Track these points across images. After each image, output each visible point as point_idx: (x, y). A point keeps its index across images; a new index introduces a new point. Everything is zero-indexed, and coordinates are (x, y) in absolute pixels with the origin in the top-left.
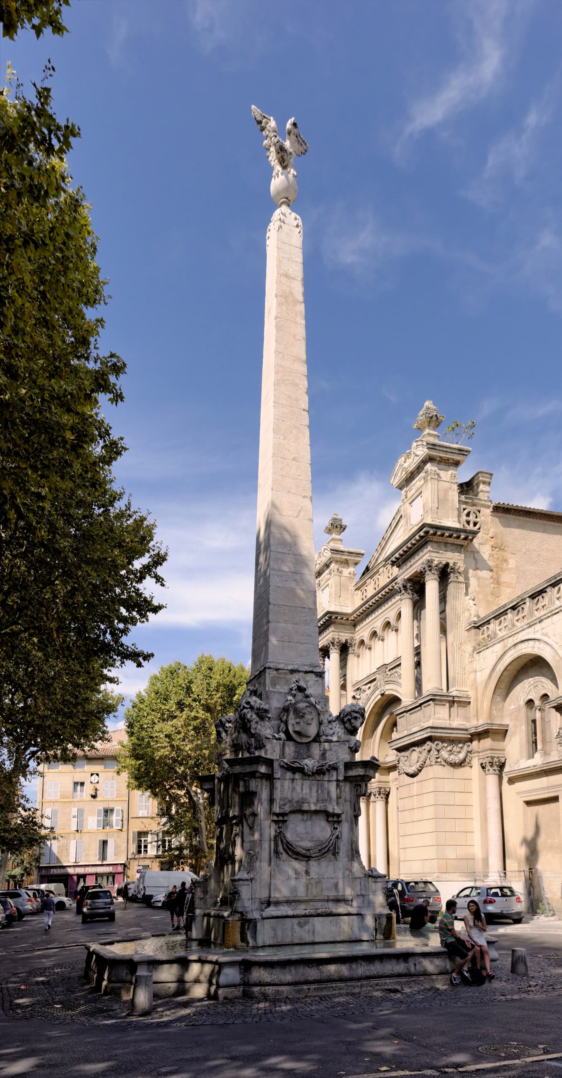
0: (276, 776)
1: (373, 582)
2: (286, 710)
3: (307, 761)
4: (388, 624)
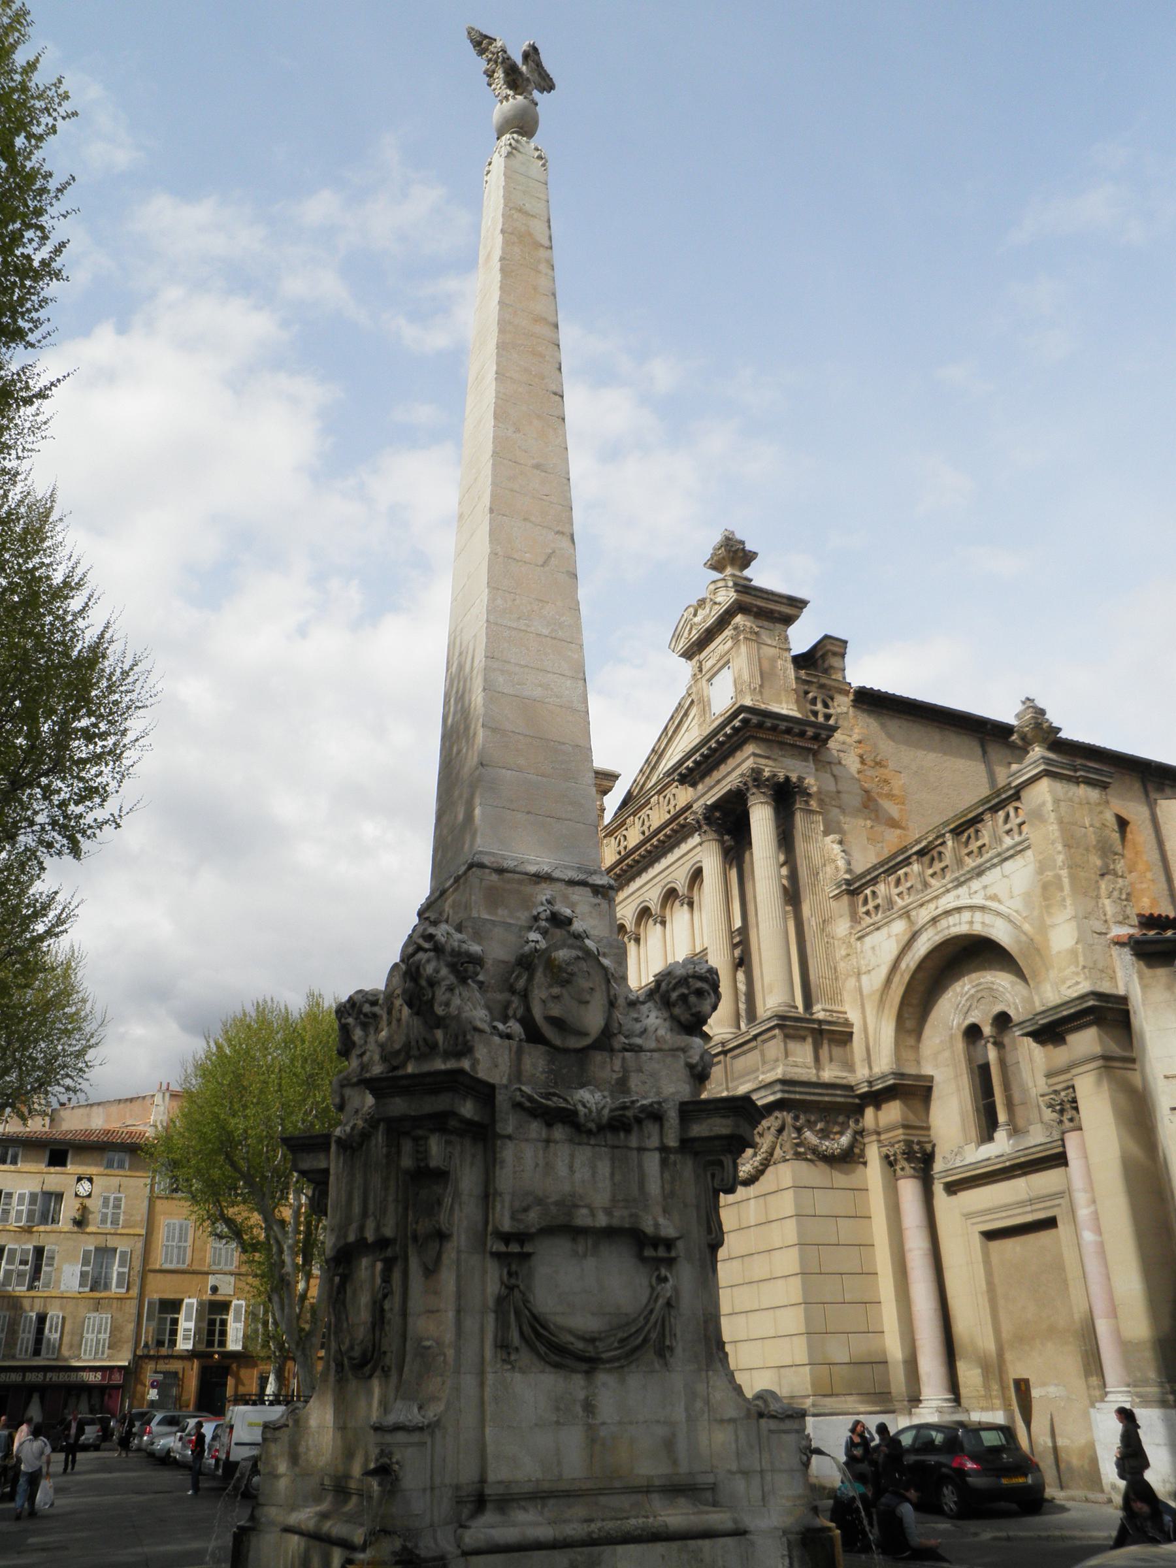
0: (500, 1128)
1: (638, 823)
2: (526, 963)
3: (584, 1094)
4: (670, 895)
